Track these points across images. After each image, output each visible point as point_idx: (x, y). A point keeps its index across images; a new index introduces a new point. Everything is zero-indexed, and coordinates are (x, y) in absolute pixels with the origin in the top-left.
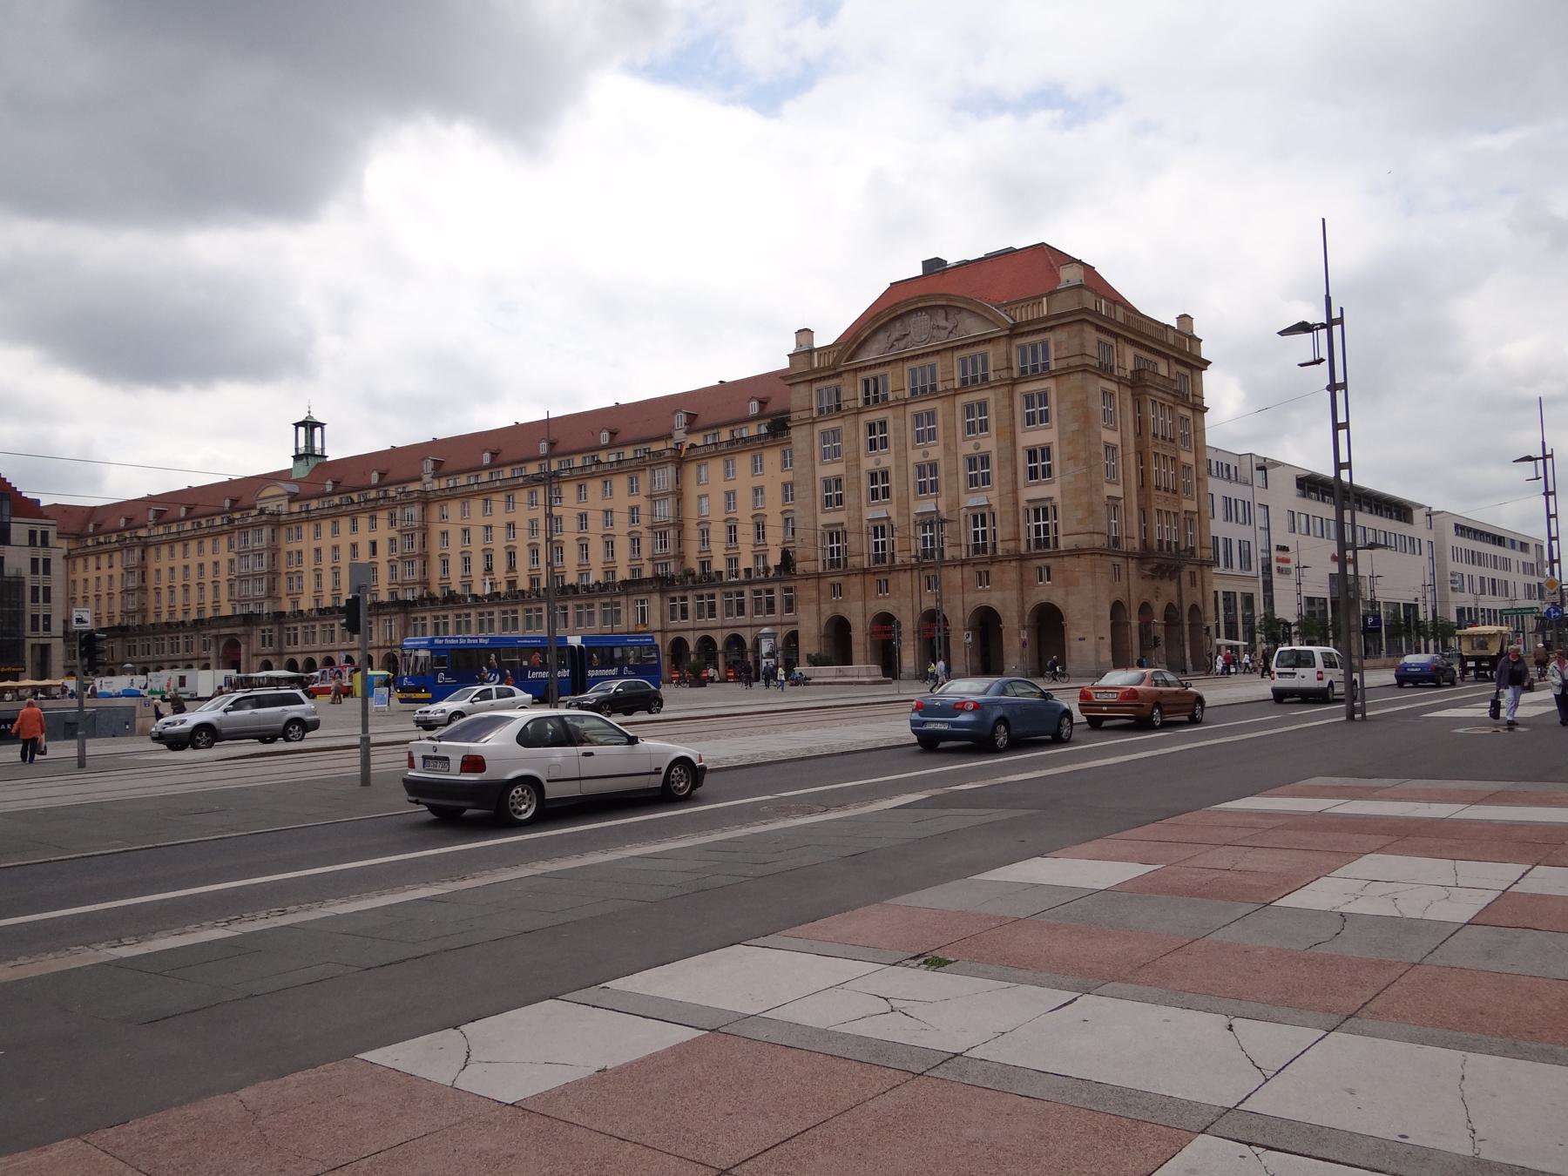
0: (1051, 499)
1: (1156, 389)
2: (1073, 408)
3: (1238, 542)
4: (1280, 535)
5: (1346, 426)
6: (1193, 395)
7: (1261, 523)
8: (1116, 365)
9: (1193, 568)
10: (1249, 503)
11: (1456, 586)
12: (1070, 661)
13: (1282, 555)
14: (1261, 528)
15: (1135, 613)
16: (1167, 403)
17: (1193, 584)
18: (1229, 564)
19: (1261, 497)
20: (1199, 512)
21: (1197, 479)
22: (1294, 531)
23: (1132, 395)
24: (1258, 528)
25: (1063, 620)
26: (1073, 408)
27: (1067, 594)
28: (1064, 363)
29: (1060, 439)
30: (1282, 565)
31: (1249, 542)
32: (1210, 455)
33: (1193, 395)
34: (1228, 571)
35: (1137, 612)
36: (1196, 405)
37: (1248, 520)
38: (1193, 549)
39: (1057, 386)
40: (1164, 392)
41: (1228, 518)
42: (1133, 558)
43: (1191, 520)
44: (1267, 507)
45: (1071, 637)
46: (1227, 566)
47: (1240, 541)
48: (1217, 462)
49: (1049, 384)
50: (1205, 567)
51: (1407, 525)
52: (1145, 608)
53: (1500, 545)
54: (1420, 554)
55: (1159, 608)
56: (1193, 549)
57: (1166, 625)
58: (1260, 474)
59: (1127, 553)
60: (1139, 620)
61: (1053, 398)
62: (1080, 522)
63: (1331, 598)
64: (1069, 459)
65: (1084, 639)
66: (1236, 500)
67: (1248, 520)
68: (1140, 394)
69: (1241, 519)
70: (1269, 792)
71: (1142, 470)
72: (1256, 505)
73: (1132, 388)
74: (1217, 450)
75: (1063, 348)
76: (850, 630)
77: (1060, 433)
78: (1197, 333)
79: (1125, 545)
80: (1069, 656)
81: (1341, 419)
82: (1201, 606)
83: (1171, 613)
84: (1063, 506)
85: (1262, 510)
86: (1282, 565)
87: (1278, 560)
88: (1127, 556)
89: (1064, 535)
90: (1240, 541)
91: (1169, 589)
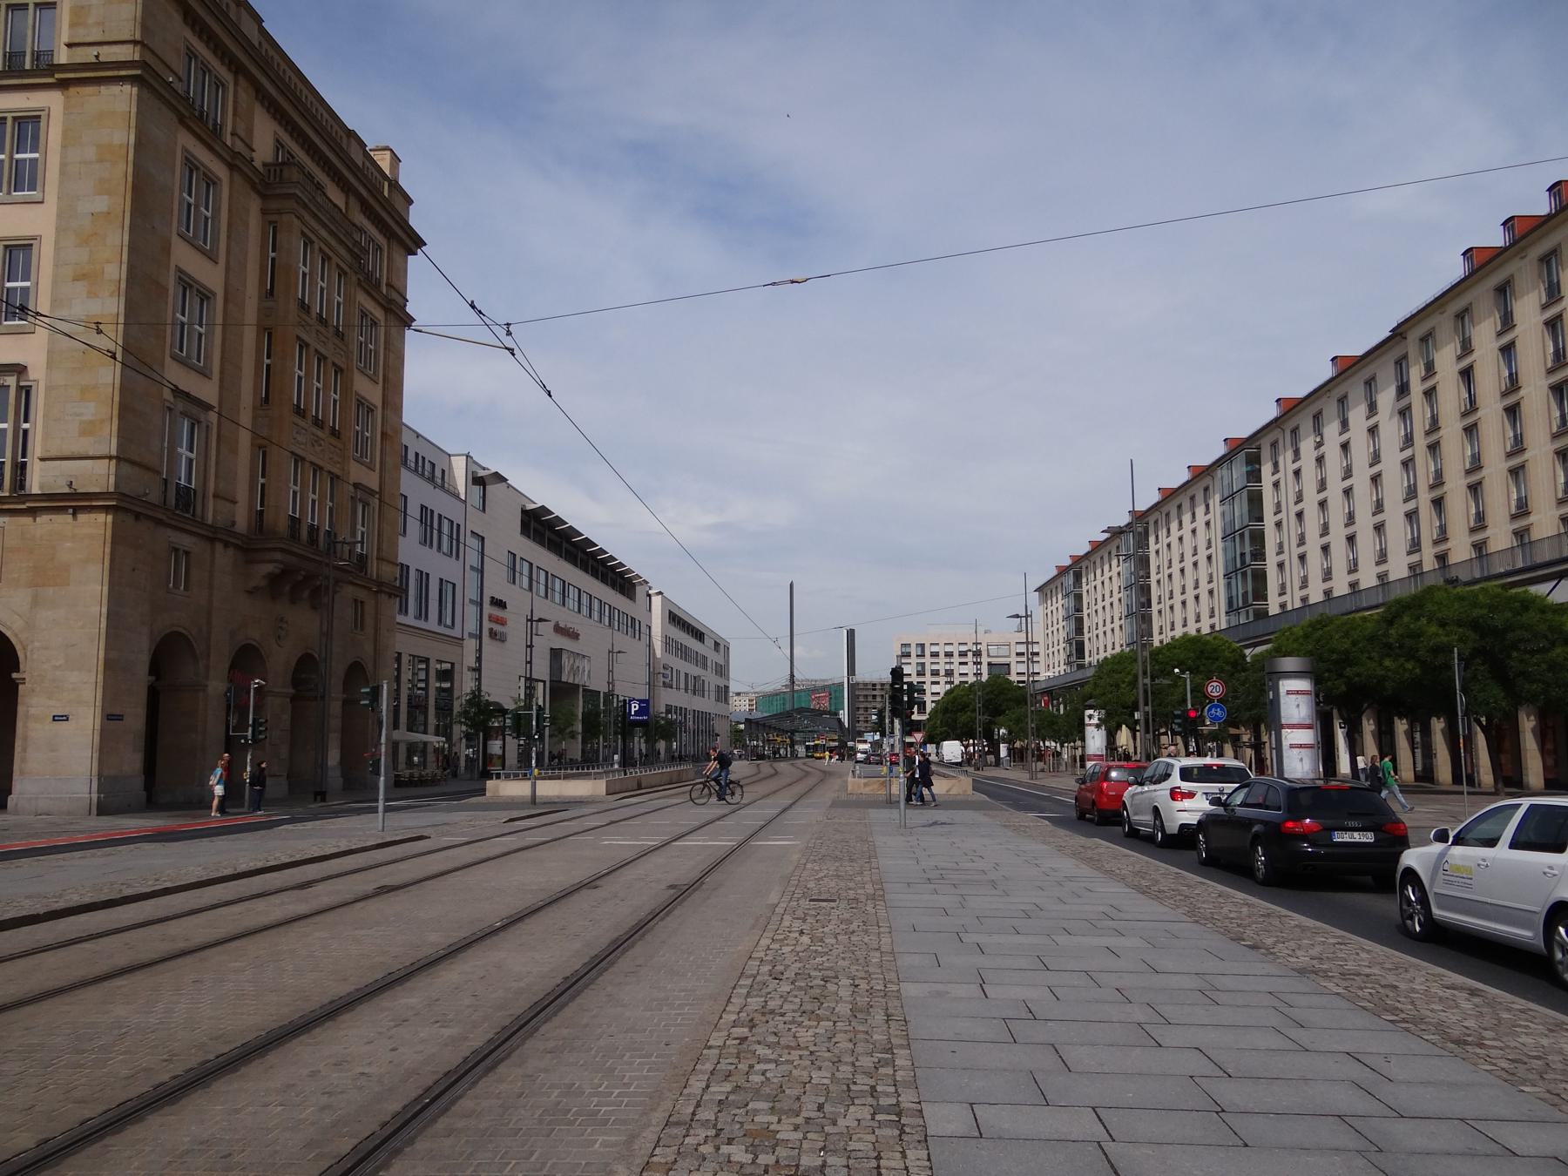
0: (19, 370)
1: (315, 216)
2: (100, 161)
3: (438, 581)
4: (497, 584)
5: (527, 663)
6: (389, 285)
7: (472, 558)
8: (229, 129)
9: (362, 595)
10: (458, 525)
11: (667, 681)
12: (22, 773)
13: (497, 612)
14: (472, 568)
15: (219, 664)
16: (335, 259)
17: (359, 623)
18: (423, 613)
19: (475, 522)
20: (380, 493)
21: (384, 434)
22: (514, 582)
23: (264, 212)
24: (467, 568)
25: (18, 670)
26: (100, 161)
27: (36, 602)
28: (87, 55)
29: (58, 230)
30: (497, 628)
31: (454, 585)
32: (406, 439)
33: (389, 285)
34: (421, 624)
35: (227, 666)
36: (391, 301)
37: (455, 551)
38: (362, 559)
39: (66, 108)
40: (331, 233)
41: (426, 541)
42: (226, 545)
43: (366, 504)
44: (483, 539)
45: (32, 711)
46: (418, 617)
47: (441, 580)
48: (417, 454)
49: (50, 102)
50: (384, 597)
51: (628, 601)
52: (246, 659)
53: (700, 641)
54: (640, 639)
55: (281, 658)
56: (362, 559)
57: (293, 699)
58: (477, 489)
59: (213, 528)
60: (231, 681)
61: (54, 134)
62: (87, 429)
63: (550, 681)
64: (76, 279)
65: (66, 718)
66: (440, 516)
67: (455, 551)
68: (279, 212)
69: (445, 547)
70: (255, 38)
71: (268, 366)
72: (468, 533)
73: (263, 197)
74: (418, 435)
75: (91, 21)
76: (38, 914)
77: (60, 216)
78: (408, 297)
79: (211, 512)
80: (24, 760)
81: (529, 665)
82: (369, 668)
83: (306, 668)
84: (49, 389)
85: (474, 640)
86: (497, 628)
87: (491, 618)
88: (215, 535)
89: (42, 459)
90: (441, 580)
91: (303, 622)
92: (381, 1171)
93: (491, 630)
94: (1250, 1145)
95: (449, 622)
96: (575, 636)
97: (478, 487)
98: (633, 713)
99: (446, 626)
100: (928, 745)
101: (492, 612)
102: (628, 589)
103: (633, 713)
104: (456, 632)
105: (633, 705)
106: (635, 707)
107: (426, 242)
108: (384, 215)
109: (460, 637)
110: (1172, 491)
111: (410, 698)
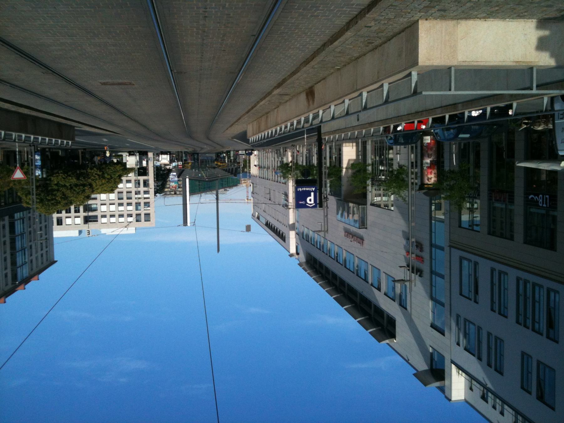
90: (476, 302)
92: (459, 134)
93: (423, 261)
94: (260, 219)
95: (465, 263)
96: (348, 233)
97: (438, 367)
98: (312, 194)
99: (469, 261)
100: (161, 156)
101: (421, 265)
102: (311, 260)
103: (312, 194)
104: (457, 254)
105: (312, 202)
106: (310, 200)
107: (413, 376)
108: (240, 74)
109: (453, 249)
110: (449, 397)
111: (511, 200)
